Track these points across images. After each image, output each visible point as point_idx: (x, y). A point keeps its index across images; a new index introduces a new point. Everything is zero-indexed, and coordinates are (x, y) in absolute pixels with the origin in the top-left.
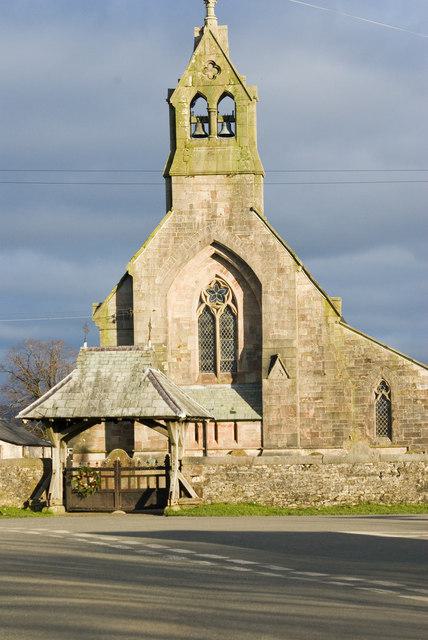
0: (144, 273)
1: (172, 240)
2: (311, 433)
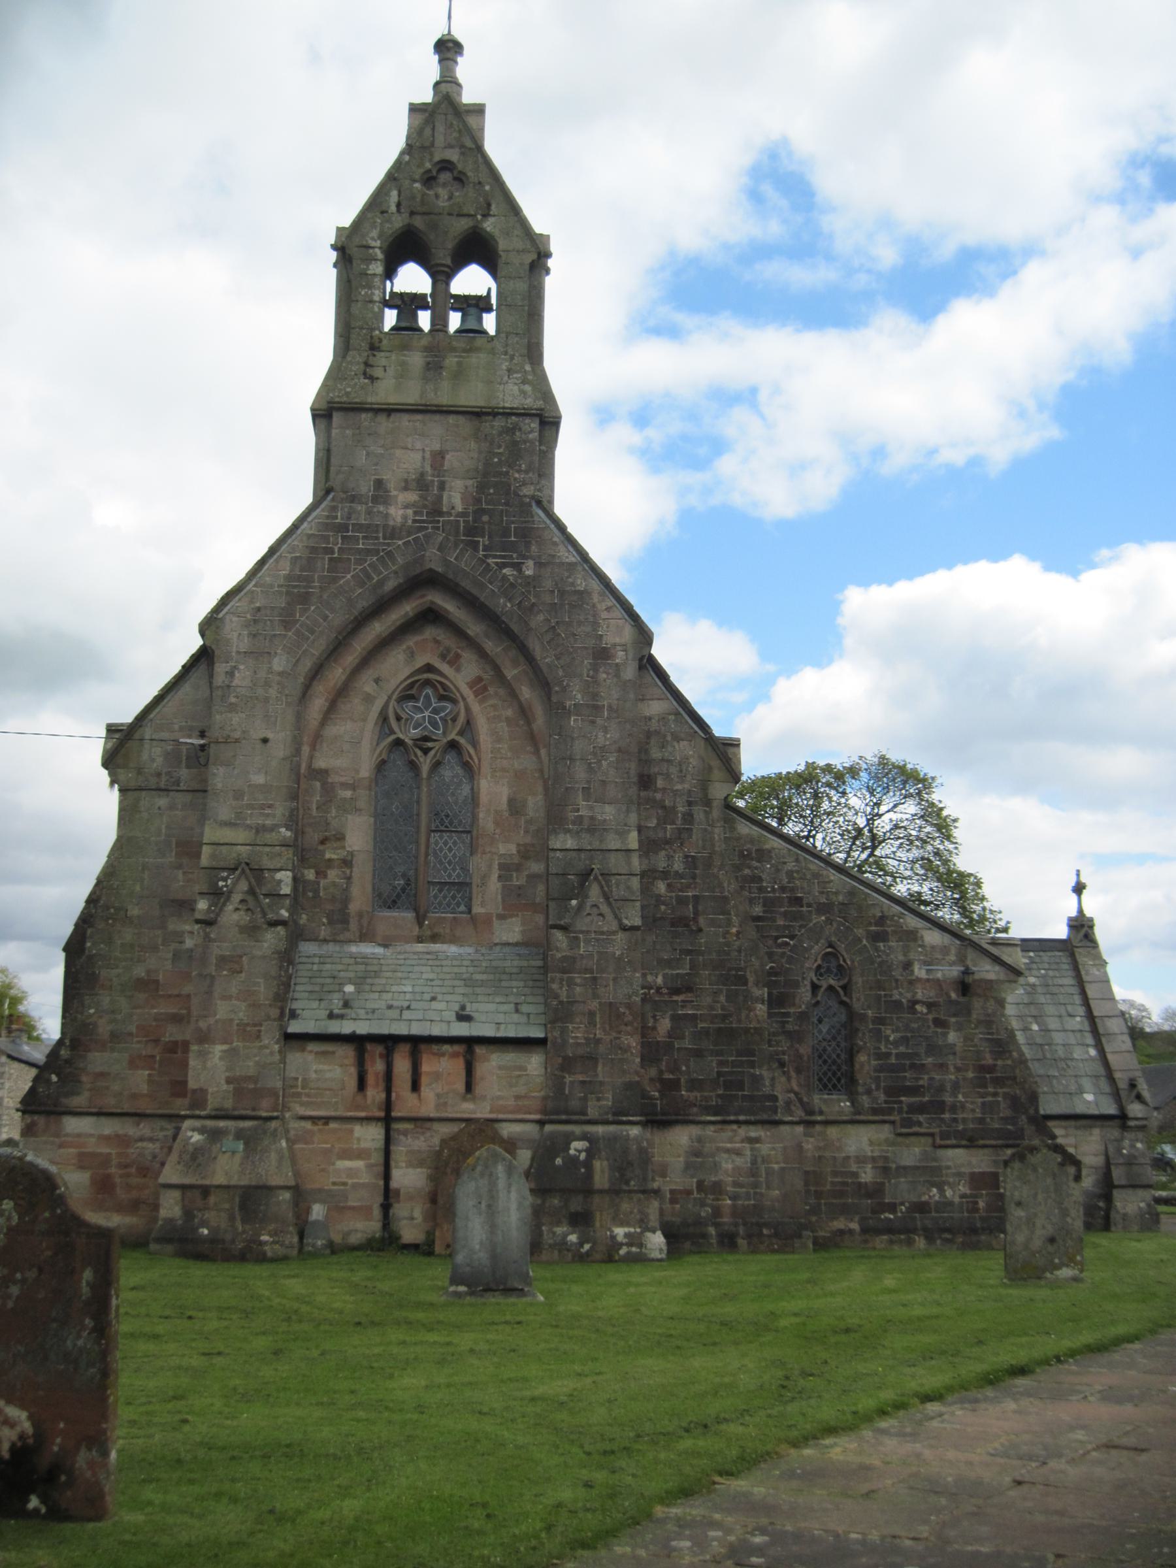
0: (245, 644)
1: (324, 563)
2: (661, 1080)
